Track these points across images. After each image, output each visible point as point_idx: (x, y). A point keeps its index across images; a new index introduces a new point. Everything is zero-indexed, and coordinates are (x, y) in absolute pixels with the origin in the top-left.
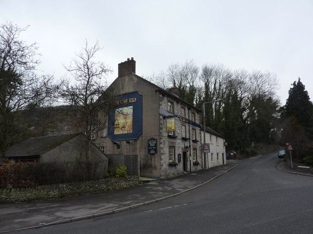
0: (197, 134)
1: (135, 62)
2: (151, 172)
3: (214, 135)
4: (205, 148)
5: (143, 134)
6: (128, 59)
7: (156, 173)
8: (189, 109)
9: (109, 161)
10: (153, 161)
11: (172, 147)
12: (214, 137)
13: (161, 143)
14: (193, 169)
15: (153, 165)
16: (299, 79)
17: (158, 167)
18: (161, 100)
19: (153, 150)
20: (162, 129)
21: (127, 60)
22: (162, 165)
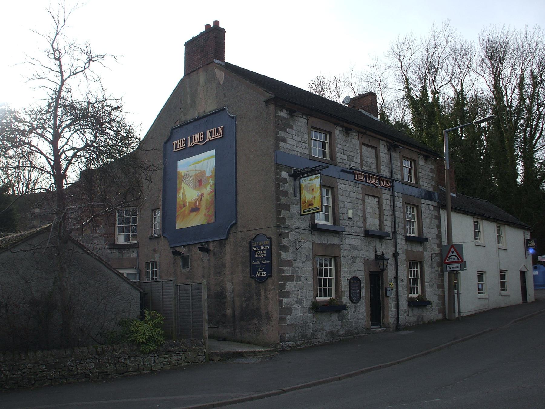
0: (426, 221)
1: (223, 31)
3: (488, 219)
4: (450, 258)
5: (239, 223)
7: (271, 332)
9: (142, 298)
10: (263, 297)
12: (488, 229)
13: (285, 248)
14: (407, 317)
15: (263, 311)
17: (275, 315)
18: (285, 126)
19: (263, 268)
20: (287, 207)
22: (287, 311)
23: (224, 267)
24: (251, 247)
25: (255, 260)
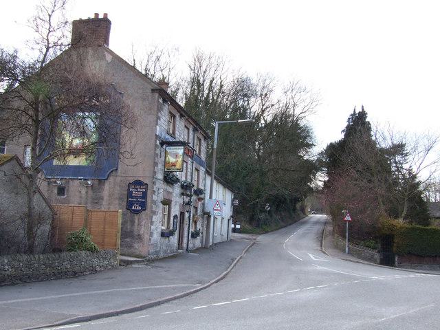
2: (131, 246)
6: (97, 15)
8: (195, 130)
10: (136, 224)
11: (44, 130)
16: (363, 107)
17: (146, 236)
21: (92, 16)
22: (151, 234)
23: (102, 199)
24: (129, 188)
25: (132, 198)
